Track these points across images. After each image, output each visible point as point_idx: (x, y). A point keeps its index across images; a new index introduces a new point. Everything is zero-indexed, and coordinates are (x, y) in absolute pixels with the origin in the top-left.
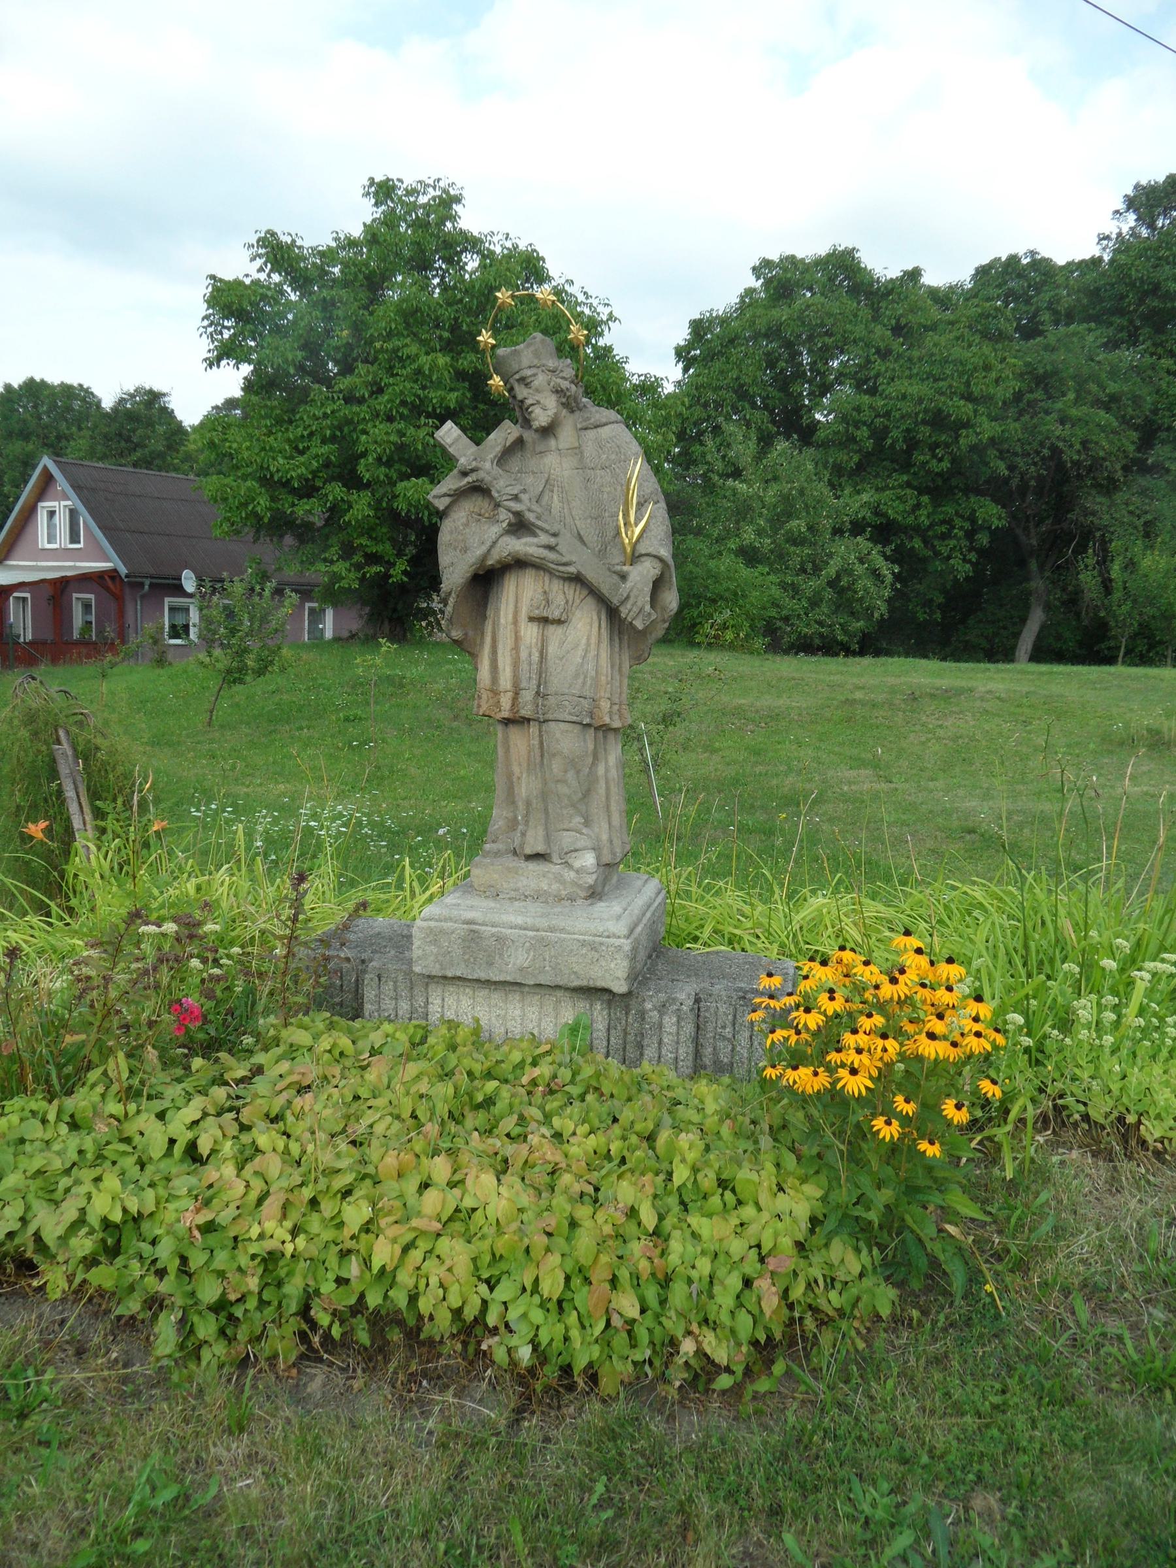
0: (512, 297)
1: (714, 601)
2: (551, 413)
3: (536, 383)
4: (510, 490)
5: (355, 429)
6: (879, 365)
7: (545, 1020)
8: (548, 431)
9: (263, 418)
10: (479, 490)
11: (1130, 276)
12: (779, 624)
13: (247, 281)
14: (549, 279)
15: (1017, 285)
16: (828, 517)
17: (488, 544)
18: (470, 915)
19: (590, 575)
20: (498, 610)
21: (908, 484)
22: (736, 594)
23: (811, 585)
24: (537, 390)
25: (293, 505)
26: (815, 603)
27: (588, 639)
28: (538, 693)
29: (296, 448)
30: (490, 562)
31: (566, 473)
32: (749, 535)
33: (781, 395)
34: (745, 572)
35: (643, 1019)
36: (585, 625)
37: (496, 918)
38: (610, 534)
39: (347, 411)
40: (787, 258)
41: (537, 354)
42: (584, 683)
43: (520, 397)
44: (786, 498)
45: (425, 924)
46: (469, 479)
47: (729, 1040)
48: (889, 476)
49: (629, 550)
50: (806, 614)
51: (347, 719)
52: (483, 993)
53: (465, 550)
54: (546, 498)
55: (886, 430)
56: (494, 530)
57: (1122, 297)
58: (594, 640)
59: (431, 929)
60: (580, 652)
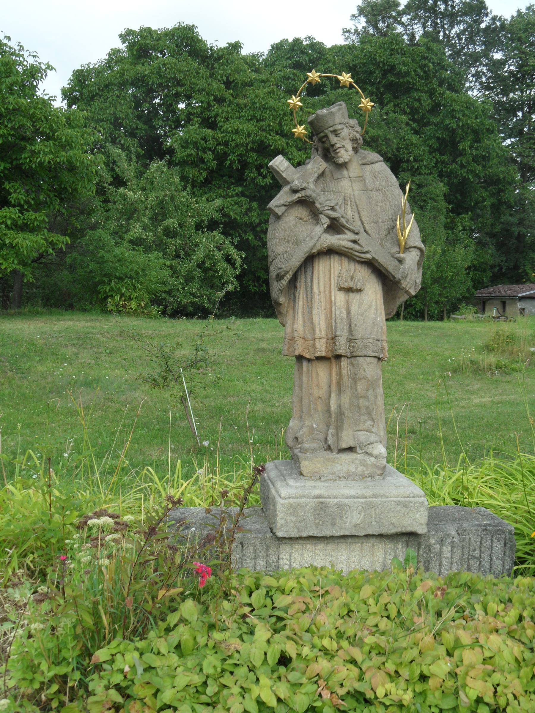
1: (121, 279)
6: (216, 108)
7: (373, 558)
10: (306, 203)
11: (375, 60)
12: (164, 295)
15: (297, 57)
16: (192, 216)
17: (316, 239)
18: (317, 492)
21: (243, 194)
22: (137, 273)
23: (186, 266)
26: (189, 279)
32: (137, 230)
33: (146, 127)
34: (141, 258)
35: (430, 550)
37: (336, 492)
40: (145, 29)
44: (161, 204)
45: (286, 501)
46: (299, 195)
47: (477, 558)
48: (228, 188)
50: (183, 289)
52: (320, 546)
55: (225, 155)
56: (319, 229)
57: (371, 73)
59: (291, 505)
60: (373, 311)
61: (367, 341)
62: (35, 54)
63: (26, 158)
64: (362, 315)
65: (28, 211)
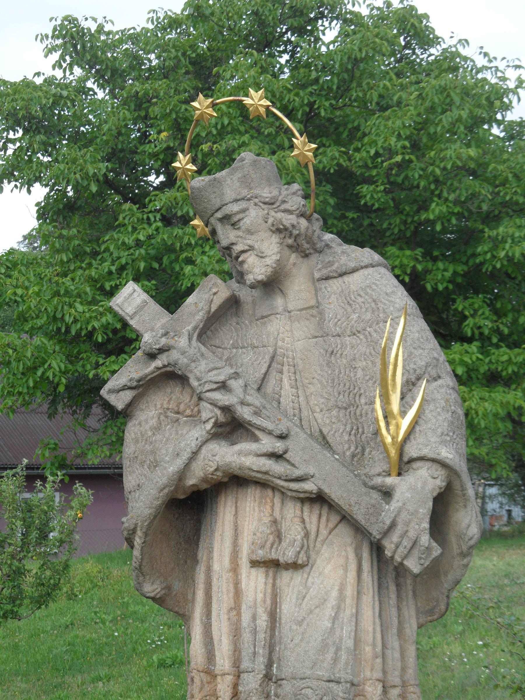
0: (213, 105)
2: (271, 261)
3: (247, 222)
4: (214, 376)
5: (177, 259)
8: (272, 285)
9: (58, 251)
10: (173, 377)
13: (39, 81)
14: (435, 41)
17: (185, 456)
19: (335, 493)
20: (210, 551)
24: (249, 232)
25: (97, 365)
27: (341, 591)
28: (268, 677)
29: (102, 289)
30: (191, 482)
31: (299, 345)
36: (335, 571)
38: (369, 431)
39: (165, 235)
41: (245, 181)
42: (336, 660)
43: (224, 243)
46: (158, 363)
49: (393, 452)
51: (162, 664)
53: (155, 465)
54: (270, 386)
58: (350, 591)
60: (329, 611)
61: (301, 684)
62: (517, 63)
63: (486, 253)
64: (300, 623)
65: (498, 347)
